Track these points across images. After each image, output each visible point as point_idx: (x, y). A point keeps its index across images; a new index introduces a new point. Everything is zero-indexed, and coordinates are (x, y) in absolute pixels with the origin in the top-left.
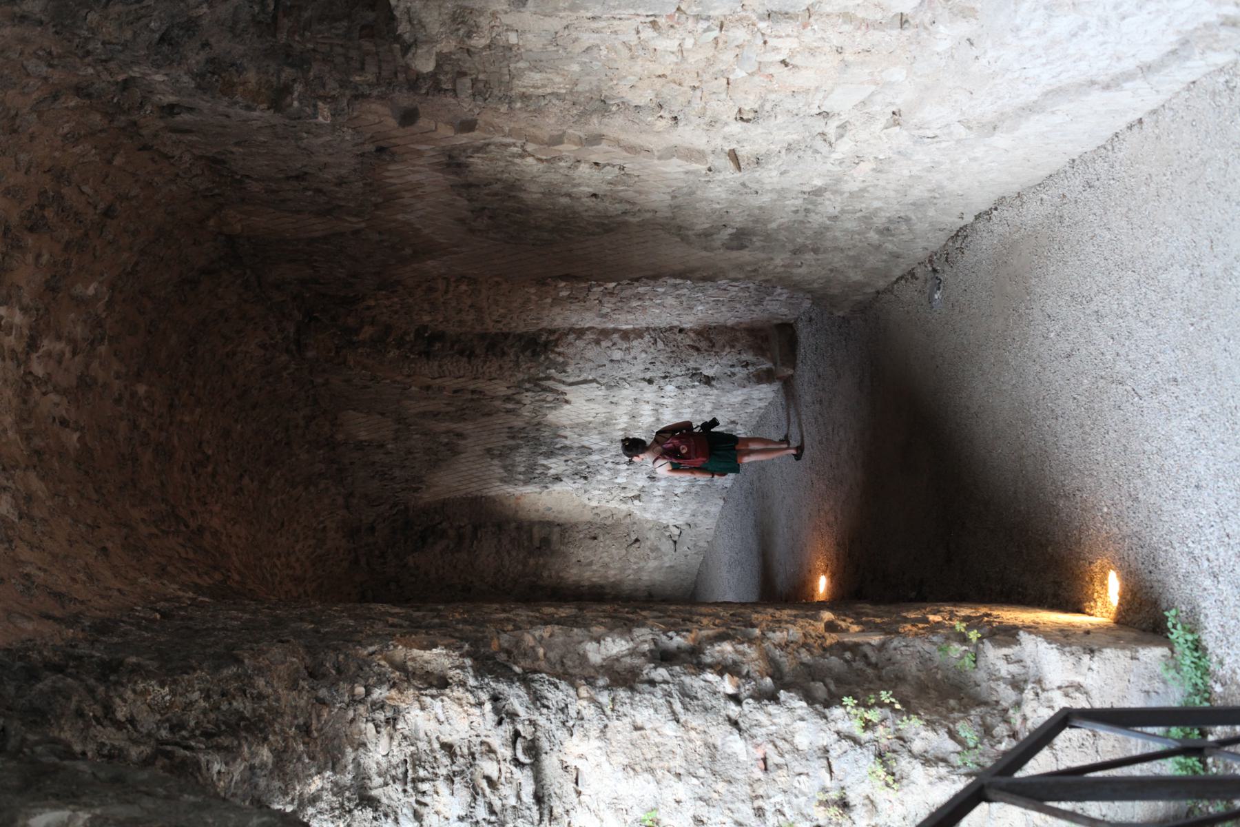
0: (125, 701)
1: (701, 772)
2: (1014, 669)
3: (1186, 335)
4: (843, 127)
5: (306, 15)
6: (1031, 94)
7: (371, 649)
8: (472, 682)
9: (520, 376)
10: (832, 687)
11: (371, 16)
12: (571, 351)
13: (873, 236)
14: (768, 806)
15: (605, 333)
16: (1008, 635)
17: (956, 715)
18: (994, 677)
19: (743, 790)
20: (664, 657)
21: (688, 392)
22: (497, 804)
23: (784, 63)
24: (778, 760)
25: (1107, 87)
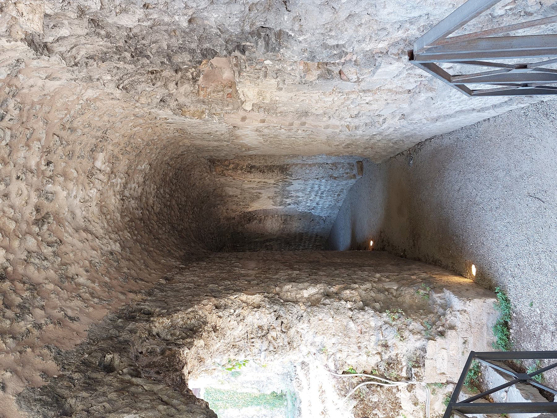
0: (155, 327)
1: (340, 334)
2: (442, 301)
3: (504, 194)
4: (385, 119)
5: (209, 90)
6: (452, 112)
7: (235, 296)
8: (268, 306)
9: (278, 178)
10: (382, 305)
11: (230, 90)
12: (294, 170)
13: (391, 144)
14: (362, 345)
15: (304, 165)
16: (439, 288)
17: (423, 317)
18: (434, 302)
19: (354, 340)
20: (328, 295)
21: (329, 182)
22: (276, 346)
23: (367, 103)
24: (365, 330)
25: (479, 111)
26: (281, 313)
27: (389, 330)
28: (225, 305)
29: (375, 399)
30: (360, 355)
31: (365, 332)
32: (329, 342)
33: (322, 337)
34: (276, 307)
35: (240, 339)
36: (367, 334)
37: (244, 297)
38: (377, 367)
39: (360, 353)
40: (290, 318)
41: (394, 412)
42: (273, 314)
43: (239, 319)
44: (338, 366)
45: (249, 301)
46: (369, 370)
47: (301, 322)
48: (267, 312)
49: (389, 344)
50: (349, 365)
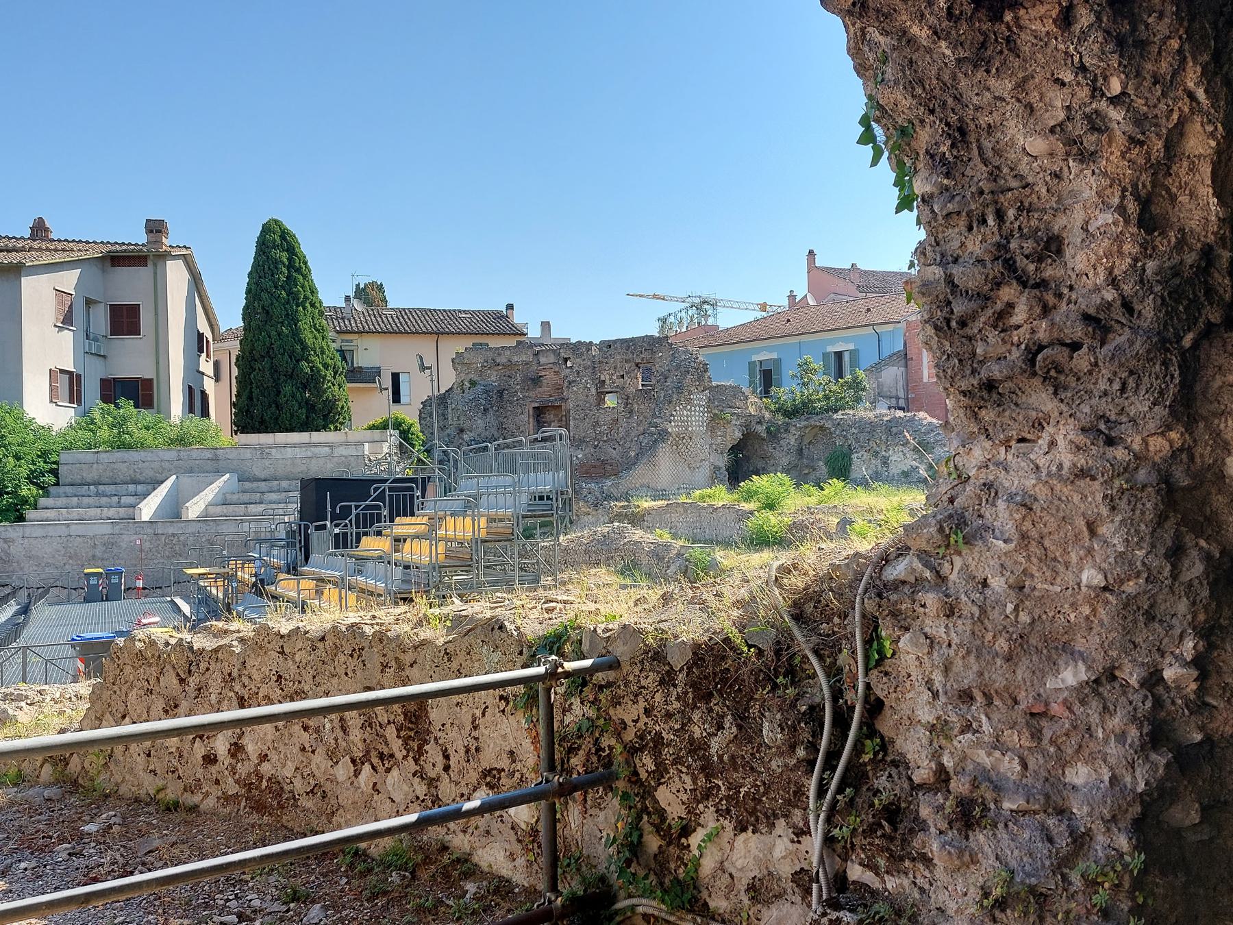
1: (1024, 617)
7: (1201, 94)
8: (1151, 266)
14: (977, 710)
19: (998, 677)
22: (973, 329)
24: (1047, 734)
26: (1120, 338)
27: (1041, 848)
28: (1142, 45)
29: (770, 732)
30: (935, 695)
31: (1037, 735)
32: (990, 563)
33: (1010, 528)
34: (1148, 310)
35: (990, 154)
36: (1026, 743)
37: (1200, 142)
38: (893, 762)
39: (943, 699)
40: (1103, 385)
41: (728, 798)
42: (1109, 295)
43: (1078, 128)
44: (894, 597)
45: (1181, 169)
46: (885, 726)
47: (1082, 439)
48: (1122, 265)
49: (980, 838)
50: (897, 641)
